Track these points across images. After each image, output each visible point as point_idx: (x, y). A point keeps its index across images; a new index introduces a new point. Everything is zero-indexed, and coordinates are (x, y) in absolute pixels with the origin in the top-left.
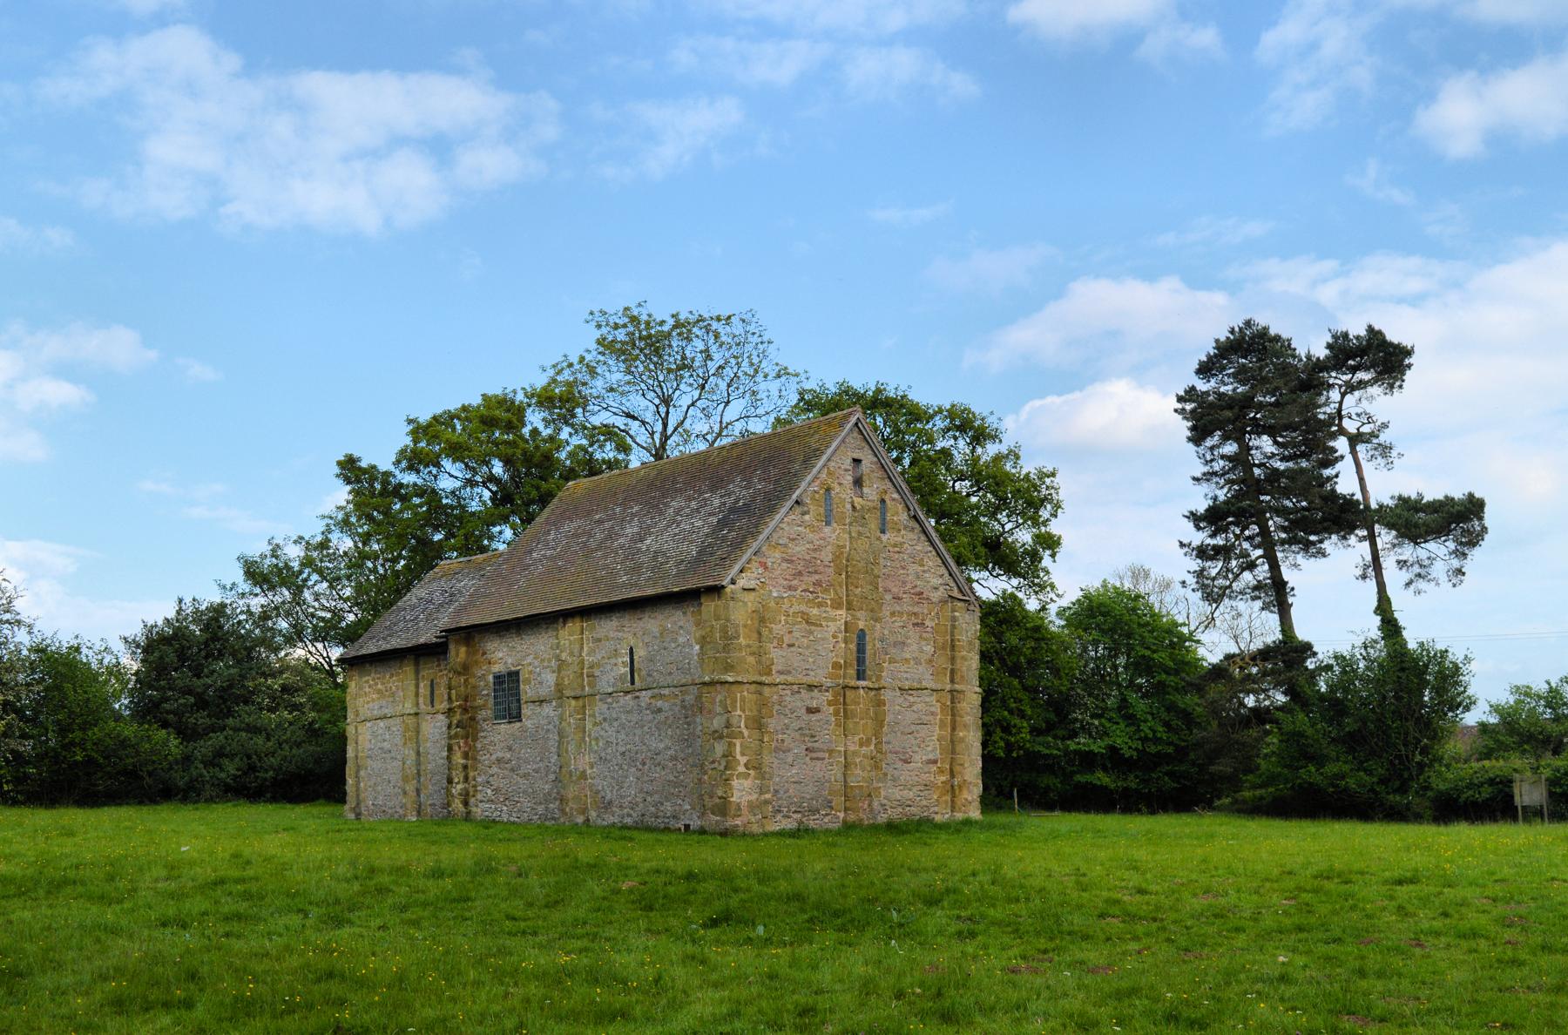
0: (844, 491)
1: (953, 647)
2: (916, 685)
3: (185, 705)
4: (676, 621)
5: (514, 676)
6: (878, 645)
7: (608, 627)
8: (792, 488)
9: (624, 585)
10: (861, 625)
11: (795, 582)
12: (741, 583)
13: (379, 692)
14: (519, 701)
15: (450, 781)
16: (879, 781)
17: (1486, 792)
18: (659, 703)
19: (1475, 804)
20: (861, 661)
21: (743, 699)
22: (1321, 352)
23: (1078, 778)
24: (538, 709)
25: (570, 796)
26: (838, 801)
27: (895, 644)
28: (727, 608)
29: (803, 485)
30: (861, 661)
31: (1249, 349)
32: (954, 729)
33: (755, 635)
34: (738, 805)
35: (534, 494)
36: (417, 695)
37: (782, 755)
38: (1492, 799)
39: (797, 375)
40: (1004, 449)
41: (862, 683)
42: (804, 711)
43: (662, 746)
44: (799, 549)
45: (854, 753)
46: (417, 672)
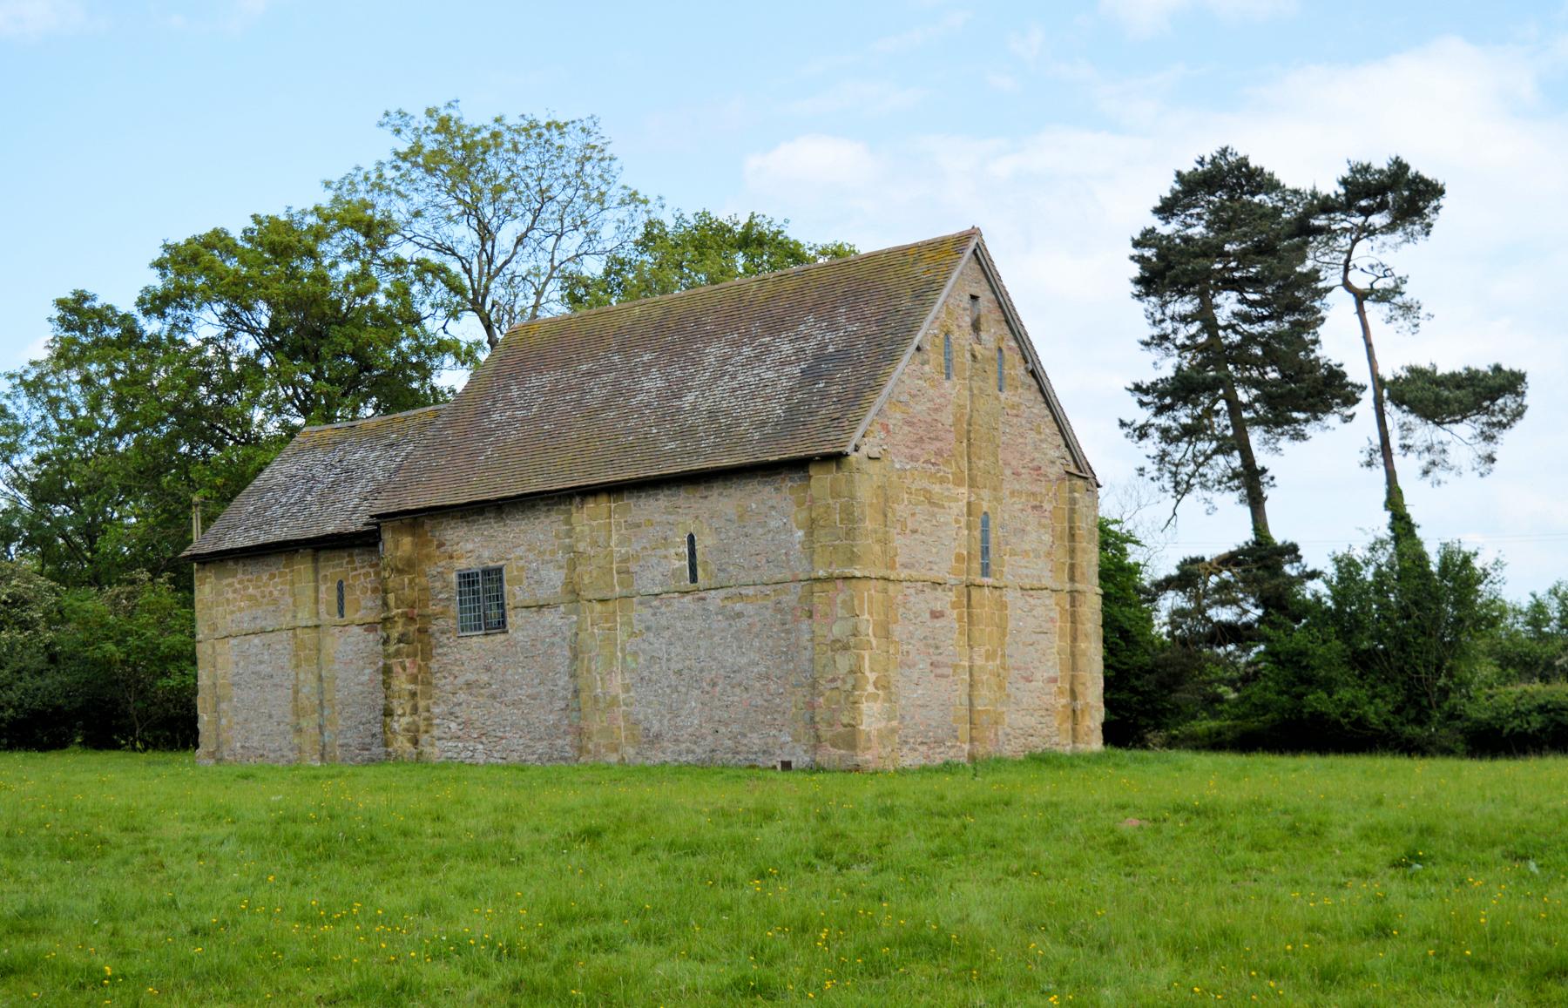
0: (962, 337)
1: (1072, 536)
2: (1036, 584)
4: (772, 504)
5: (494, 575)
7: (652, 508)
8: (911, 331)
9: (673, 454)
10: (985, 506)
11: (917, 451)
13: (251, 598)
14: (501, 606)
15: (388, 713)
17: (1537, 721)
18: (738, 607)
19: (1524, 734)
21: (871, 597)
22: (1330, 187)
24: (535, 617)
25: (595, 727)
28: (850, 482)
31: (1224, 184)
33: (881, 517)
34: (868, 734)
35: (349, 345)
36: (317, 601)
37: (907, 671)
38: (1542, 730)
39: (646, 202)
43: (744, 660)
44: (920, 408)
45: (982, 668)
46: (316, 571)
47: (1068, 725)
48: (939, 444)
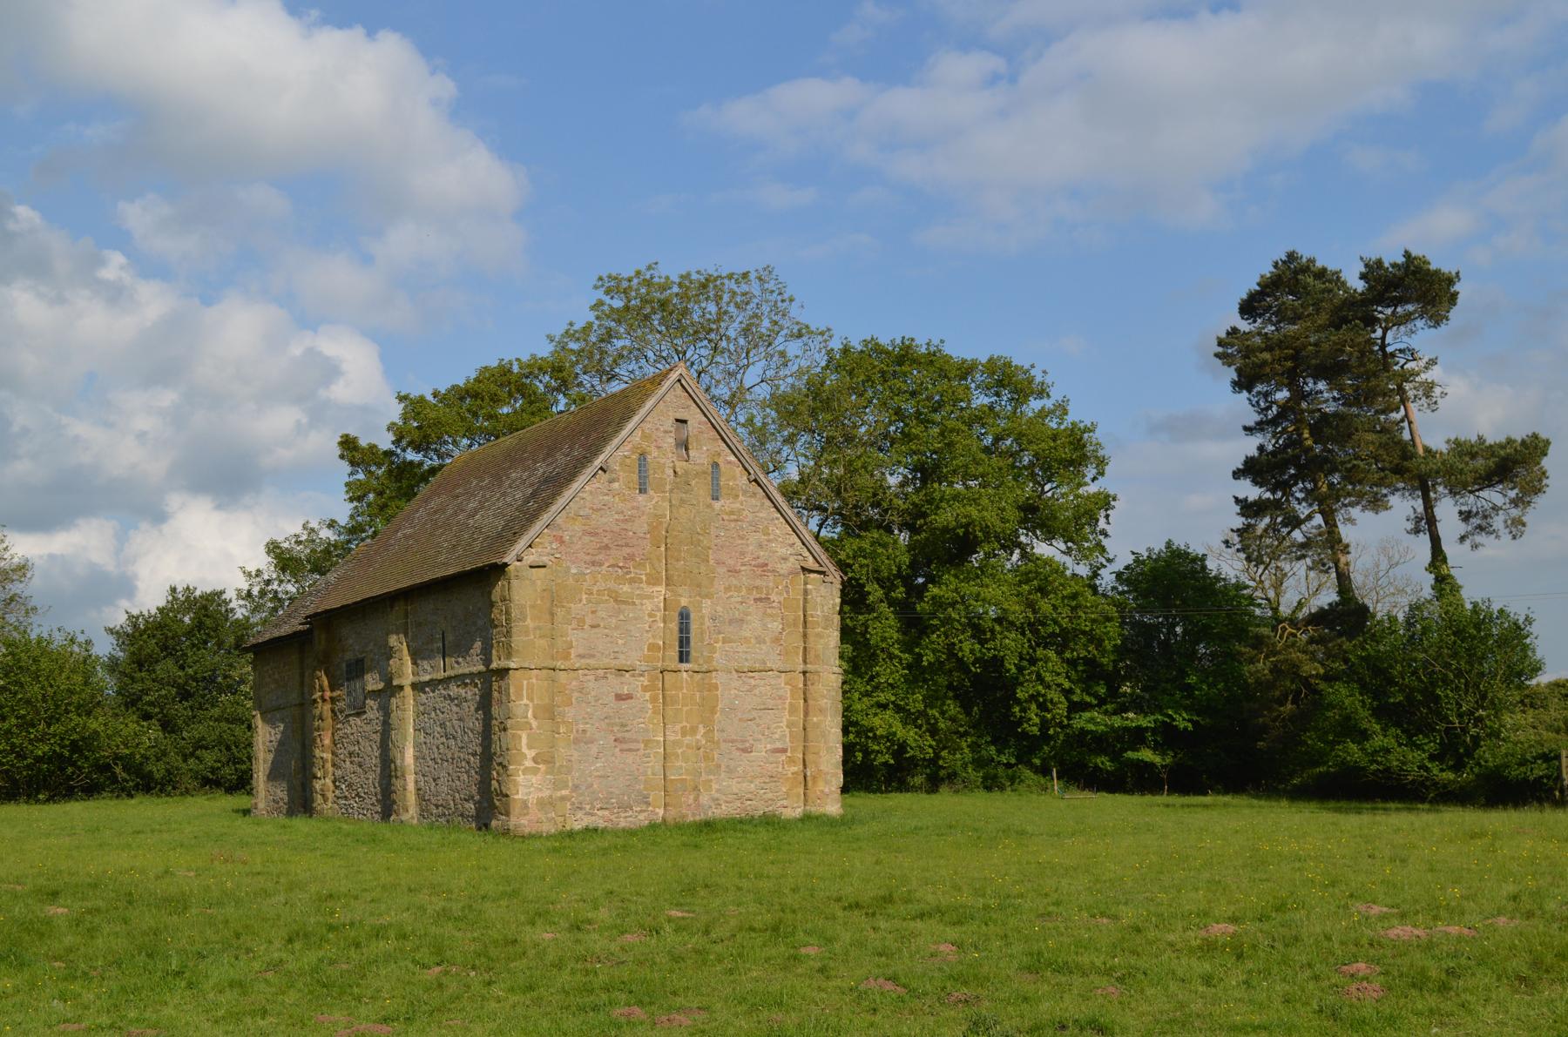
0: (664, 456)
3: (165, 697)
6: (708, 623)
10: (684, 602)
12: (530, 558)
16: (710, 772)
20: (684, 642)
23: (1130, 754)
26: (657, 796)
27: (731, 622)
29: (608, 449)
30: (684, 642)
32: (806, 714)
40: (1048, 403)
41: (684, 666)
42: (612, 697)
45: (676, 743)
47: (801, 790)
48: (628, 550)
